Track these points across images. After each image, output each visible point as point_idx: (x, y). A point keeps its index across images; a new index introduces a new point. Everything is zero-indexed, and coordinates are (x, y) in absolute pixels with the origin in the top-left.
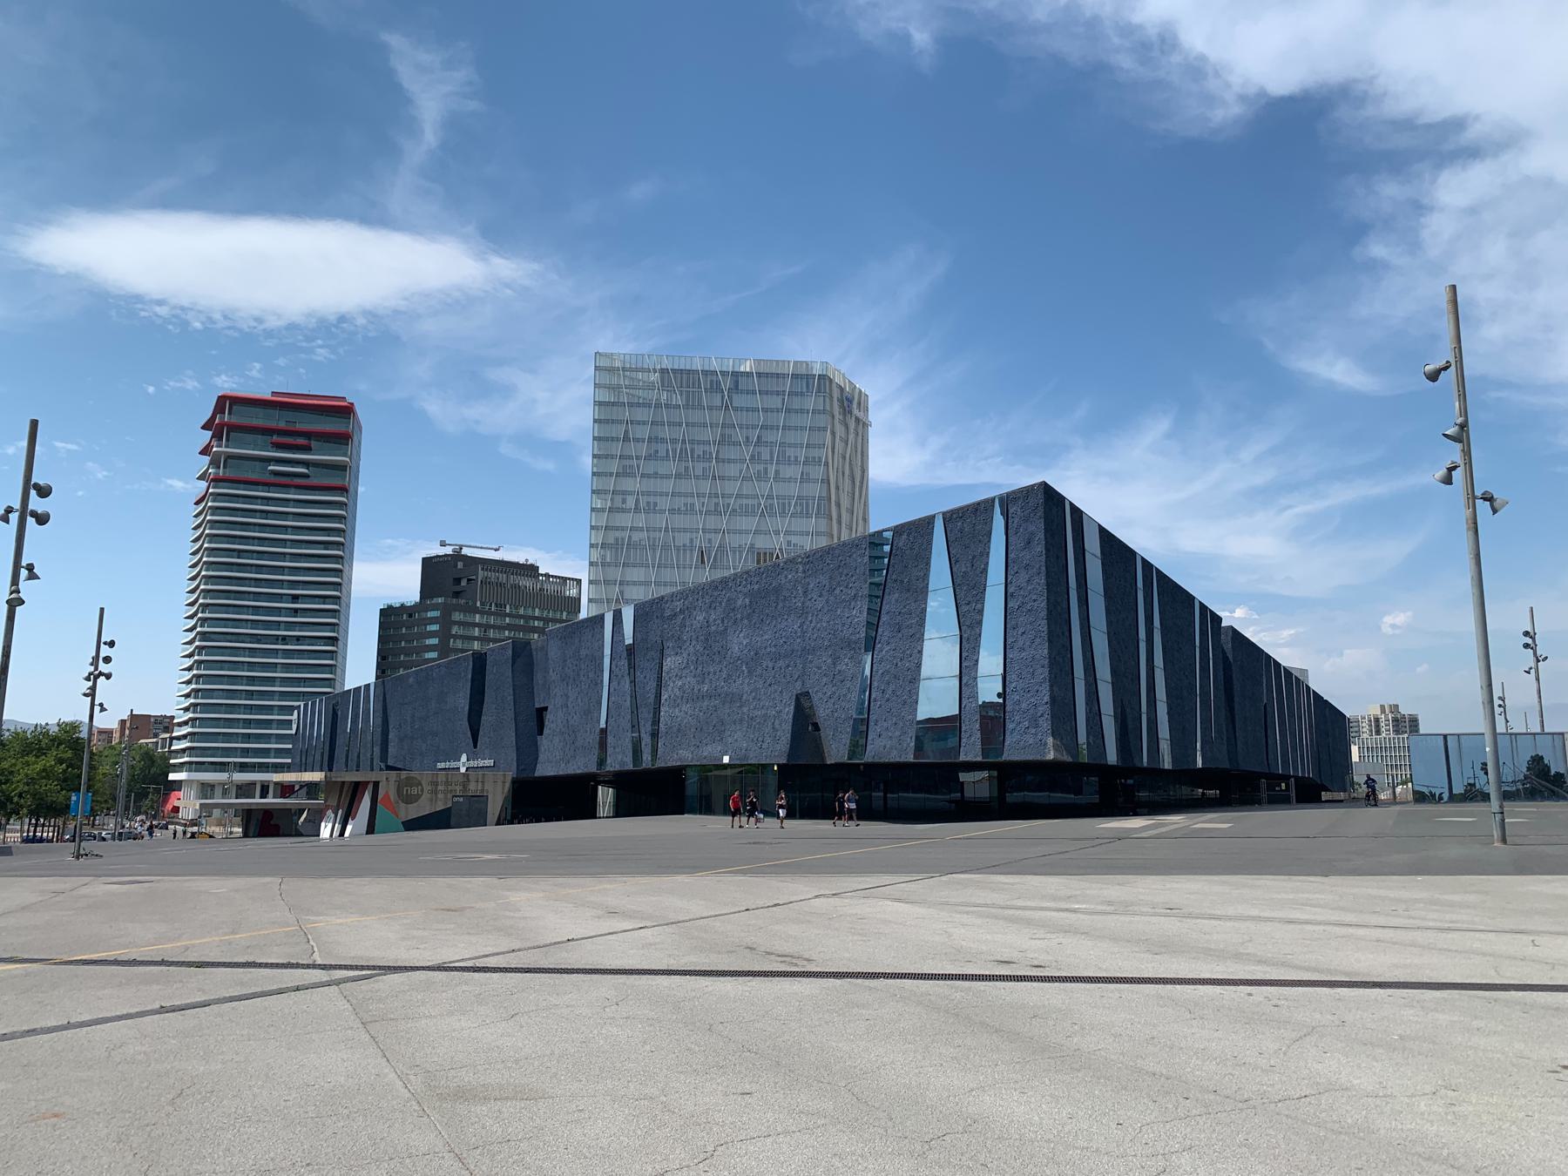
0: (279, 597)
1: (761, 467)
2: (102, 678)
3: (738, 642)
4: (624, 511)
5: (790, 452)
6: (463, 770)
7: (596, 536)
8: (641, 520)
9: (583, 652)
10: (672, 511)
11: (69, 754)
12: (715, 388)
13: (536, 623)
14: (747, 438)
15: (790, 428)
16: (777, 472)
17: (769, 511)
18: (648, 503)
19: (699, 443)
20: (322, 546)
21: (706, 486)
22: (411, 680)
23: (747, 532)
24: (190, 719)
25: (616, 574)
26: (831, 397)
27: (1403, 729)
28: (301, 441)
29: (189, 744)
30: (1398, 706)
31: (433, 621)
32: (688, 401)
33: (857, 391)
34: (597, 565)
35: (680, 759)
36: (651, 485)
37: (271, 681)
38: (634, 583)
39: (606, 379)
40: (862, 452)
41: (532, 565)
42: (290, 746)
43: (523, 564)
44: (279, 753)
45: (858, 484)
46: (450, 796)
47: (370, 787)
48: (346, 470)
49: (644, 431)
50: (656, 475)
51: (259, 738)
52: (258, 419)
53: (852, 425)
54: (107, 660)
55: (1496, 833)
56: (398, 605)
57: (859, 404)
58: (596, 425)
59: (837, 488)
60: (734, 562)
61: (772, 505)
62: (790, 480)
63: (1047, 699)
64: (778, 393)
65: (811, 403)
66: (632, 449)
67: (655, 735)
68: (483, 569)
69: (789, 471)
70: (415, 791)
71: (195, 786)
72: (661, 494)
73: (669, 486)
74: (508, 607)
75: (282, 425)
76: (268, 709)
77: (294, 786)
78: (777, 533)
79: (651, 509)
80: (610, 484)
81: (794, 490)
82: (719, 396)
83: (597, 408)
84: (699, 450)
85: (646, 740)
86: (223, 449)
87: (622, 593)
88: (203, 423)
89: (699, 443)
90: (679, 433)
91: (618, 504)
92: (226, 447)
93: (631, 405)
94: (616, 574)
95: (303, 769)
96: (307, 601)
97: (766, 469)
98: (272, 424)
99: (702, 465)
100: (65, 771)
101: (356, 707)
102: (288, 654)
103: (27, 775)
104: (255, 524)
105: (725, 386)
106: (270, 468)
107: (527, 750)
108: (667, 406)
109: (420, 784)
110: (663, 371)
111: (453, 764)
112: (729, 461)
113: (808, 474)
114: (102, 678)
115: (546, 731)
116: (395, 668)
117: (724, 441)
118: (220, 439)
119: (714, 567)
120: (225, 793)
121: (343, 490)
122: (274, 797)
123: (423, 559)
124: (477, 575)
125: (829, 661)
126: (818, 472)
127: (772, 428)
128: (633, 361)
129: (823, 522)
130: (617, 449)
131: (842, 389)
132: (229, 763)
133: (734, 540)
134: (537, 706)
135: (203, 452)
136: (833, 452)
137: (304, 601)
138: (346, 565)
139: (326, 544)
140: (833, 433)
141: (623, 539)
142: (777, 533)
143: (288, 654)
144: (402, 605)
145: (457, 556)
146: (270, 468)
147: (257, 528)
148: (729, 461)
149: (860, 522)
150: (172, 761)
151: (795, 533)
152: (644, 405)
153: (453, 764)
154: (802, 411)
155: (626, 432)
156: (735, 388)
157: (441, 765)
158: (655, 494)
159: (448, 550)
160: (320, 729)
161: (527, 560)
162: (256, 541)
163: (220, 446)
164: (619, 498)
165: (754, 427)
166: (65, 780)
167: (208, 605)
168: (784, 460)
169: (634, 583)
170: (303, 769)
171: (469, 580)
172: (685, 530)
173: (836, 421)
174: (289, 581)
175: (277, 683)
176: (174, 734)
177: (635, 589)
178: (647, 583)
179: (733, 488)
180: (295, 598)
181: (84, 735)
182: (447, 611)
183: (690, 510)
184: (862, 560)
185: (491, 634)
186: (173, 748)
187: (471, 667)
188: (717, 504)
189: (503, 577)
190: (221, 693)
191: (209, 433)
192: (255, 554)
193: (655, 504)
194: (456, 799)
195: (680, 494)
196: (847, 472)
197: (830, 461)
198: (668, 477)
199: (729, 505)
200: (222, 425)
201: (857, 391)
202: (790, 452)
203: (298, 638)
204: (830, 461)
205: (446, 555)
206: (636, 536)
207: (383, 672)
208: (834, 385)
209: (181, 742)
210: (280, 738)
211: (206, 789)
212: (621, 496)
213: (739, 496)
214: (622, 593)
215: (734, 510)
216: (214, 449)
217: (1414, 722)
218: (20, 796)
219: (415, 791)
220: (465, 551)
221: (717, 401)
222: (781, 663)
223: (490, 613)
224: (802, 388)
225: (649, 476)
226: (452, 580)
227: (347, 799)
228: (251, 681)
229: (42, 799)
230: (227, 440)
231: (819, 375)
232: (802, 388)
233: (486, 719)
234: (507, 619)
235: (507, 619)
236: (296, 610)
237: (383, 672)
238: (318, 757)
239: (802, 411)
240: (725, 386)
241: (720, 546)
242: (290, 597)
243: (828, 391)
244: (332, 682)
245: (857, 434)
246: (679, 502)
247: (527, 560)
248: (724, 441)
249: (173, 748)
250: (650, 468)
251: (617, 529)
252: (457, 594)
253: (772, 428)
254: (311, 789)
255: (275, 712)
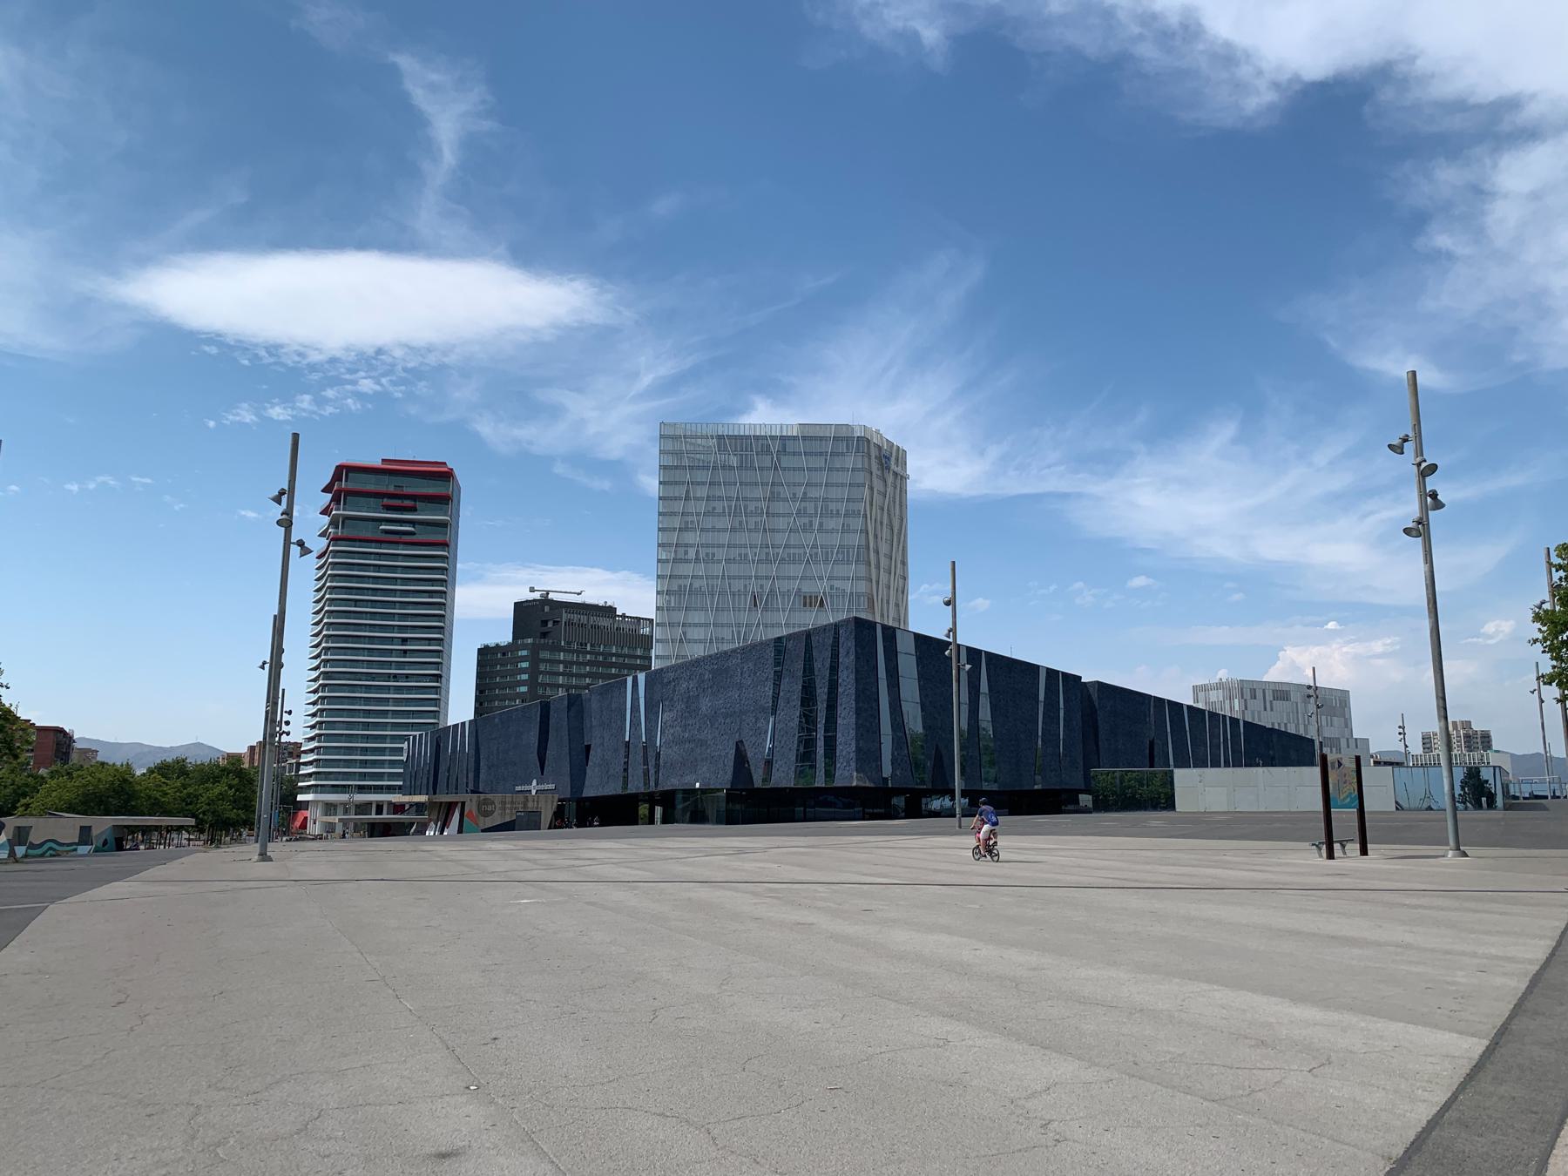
0: (391, 640)
1: (806, 520)
2: (284, 735)
3: (705, 704)
4: (687, 561)
5: (833, 506)
6: (534, 792)
7: (662, 585)
8: (701, 570)
9: (613, 706)
10: (728, 561)
11: (236, 781)
12: (766, 451)
13: (614, 659)
14: (794, 494)
15: (832, 485)
16: (821, 524)
17: (812, 559)
18: (707, 554)
19: (752, 499)
20: (427, 595)
21: (758, 538)
22: (497, 720)
23: (795, 578)
24: (316, 748)
25: (680, 617)
26: (869, 456)
27: (1476, 745)
28: (408, 503)
29: (314, 770)
30: (1470, 722)
31: (523, 659)
32: (742, 462)
33: (895, 448)
34: (663, 610)
35: (672, 785)
36: (709, 538)
37: (384, 713)
38: (695, 625)
39: (669, 446)
40: (901, 502)
41: (610, 607)
42: (402, 771)
43: (602, 607)
44: (392, 776)
45: (896, 531)
46: (514, 811)
47: (460, 805)
48: (447, 527)
49: (702, 492)
50: (713, 529)
51: (374, 763)
52: (371, 484)
53: (890, 479)
54: (287, 723)
55: (957, 825)
56: (493, 645)
57: (897, 459)
58: (661, 486)
59: (876, 536)
60: (783, 604)
61: (816, 554)
62: (832, 531)
63: (854, 749)
64: (821, 454)
65: (849, 462)
66: (692, 507)
67: (657, 766)
68: (566, 612)
69: (831, 523)
70: (490, 808)
71: (320, 805)
72: (719, 546)
73: (725, 538)
74: (589, 645)
75: (391, 489)
76: (383, 738)
77: (404, 806)
78: (821, 578)
79: (711, 559)
80: (674, 537)
81: (836, 540)
82: (770, 457)
83: (662, 471)
84: (751, 507)
85: (652, 771)
86: (341, 512)
87: (685, 633)
88: (322, 488)
89: (752, 499)
90: (733, 493)
91: (681, 555)
92: (343, 510)
93: (692, 468)
94: (680, 617)
95: (413, 793)
96: (419, 643)
97: (811, 522)
98: (382, 489)
99: (754, 519)
100: (234, 794)
101: (454, 739)
102: (399, 689)
103: (208, 798)
104: (369, 577)
105: (774, 449)
106: (381, 527)
107: (578, 776)
108: (724, 467)
109: (493, 803)
110: (720, 437)
111: (527, 788)
112: (779, 515)
113: (848, 525)
114: (284, 735)
115: (590, 763)
116: (491, 710)
117: (773, 498)
118: (338, 503)
119: (765, 609)
120: (346, 812)
121: (444, 545)
122: (388, 814)
123: (515, 603)
124: (561, 618)
125: (754, 720)
126: (857, 523)
127: (816, 485)
128: (694, 429)
129: (862, 568)
130: (679, 506)
131: (880, 448)
132: (349, 785)
133: (784, 586)
134: (586, 743)
135: (324, 512)
136: (871, 505)
137: (412, 643)
138: (449, 588)
139: (431, 593)
140: (871, 489)
141: (686, 586)
142: (821, 578)
143: (399, 689)
144: (497, 645)
145: (545, 601)
146: (381, 527)
147: (370, 592)
148: (779, 515)
149: (899, 565)
150: (300, 784)
151: (837, 579)
152: (704, 468)
153: (527, 788)
154: (843, 469)
155: (687, 492)
156: (783, 451)
157: (518, 788)
158: (713, 546)
159: (537, 596)
160: (427, 751)
161: (606, 602)
162: (369, 603)
163: (338, 509)
164: (682, 551)
165: (800, 485)
166: (235, 802)
167: (329, 648)
168: (827, 513)
169: (695, 625)
170: (413, 793)
171: (554, 622)
172: (740, 578)
173: (874, 476)
174: (399, 614)
175: (390, 715)
176: (301, 761)
177: (696, 630)
178: (707, 625)
179: (781, 539)
180: (404, 641)
181: (246, 766)
182: (534, 650)
183: (744, 559)
184: (770, 653)
185: (574, 669)
186: (300, 773)
187: (539, 713)
188: (767, 554)
189: (584, 619)
190: (342, 725)
191: (329, 496)
192: (369, 615)
193: (714, 555)
194: (518, 814)
195: (735, 546)
196: (885, 521)
197: (868, 513)
198: (725, 530)
199: (778, 554)
200: (339, 492)
201: (895, 448)
202: (833, 506)
203: (407, 676)
204: (868, 513)
205: (534, 600)
206: (697, 584)
207: (481, 704)
208: (872, 445)
209: (308, 767)
210: (393, 763)
211: (330, 808)
212: (683, 549)
213: (787, 546)
214: (685, 633)
215: (783, 559)
216: (334, 512)
217: (1486, 739)
218: (204, 813)
219: (490, 808)
220: (551, 596)
221: (767, 461)
222: (728, 720)
223: (573, 652)
224: (843, 449)
225: (707, 530)
226: (540, 622)
227: (444, 814)
228: (368, 713)
229: (219, 816)
230: (344, 504)
231: (858, 437)
232: (843, 449)
233: (551, 753)
234: (588, 656)
235: (588, 656)
236: (405, 651)
237: (481, 704)
238: (425, 781)
239: (843, 469)
240: (774, 449)
241: (771, 591)
242: (400, 640)
243: (866, 451)
244: (437, 714)
245: (895, 488)
246: (734, 553)
247: (606, 602)
248: (773, 498)
249: (300, 773)
250: (709, 522)
251: (680, 577)
252: (544, 635)
253: (816, 485)
254: (419, 808)
255: (389, 728)
